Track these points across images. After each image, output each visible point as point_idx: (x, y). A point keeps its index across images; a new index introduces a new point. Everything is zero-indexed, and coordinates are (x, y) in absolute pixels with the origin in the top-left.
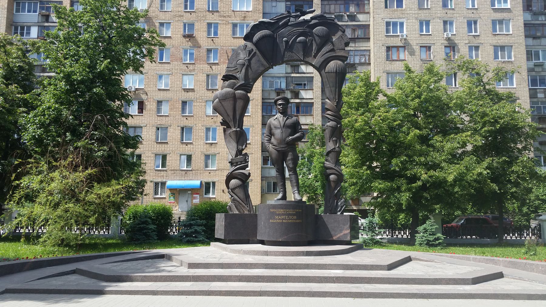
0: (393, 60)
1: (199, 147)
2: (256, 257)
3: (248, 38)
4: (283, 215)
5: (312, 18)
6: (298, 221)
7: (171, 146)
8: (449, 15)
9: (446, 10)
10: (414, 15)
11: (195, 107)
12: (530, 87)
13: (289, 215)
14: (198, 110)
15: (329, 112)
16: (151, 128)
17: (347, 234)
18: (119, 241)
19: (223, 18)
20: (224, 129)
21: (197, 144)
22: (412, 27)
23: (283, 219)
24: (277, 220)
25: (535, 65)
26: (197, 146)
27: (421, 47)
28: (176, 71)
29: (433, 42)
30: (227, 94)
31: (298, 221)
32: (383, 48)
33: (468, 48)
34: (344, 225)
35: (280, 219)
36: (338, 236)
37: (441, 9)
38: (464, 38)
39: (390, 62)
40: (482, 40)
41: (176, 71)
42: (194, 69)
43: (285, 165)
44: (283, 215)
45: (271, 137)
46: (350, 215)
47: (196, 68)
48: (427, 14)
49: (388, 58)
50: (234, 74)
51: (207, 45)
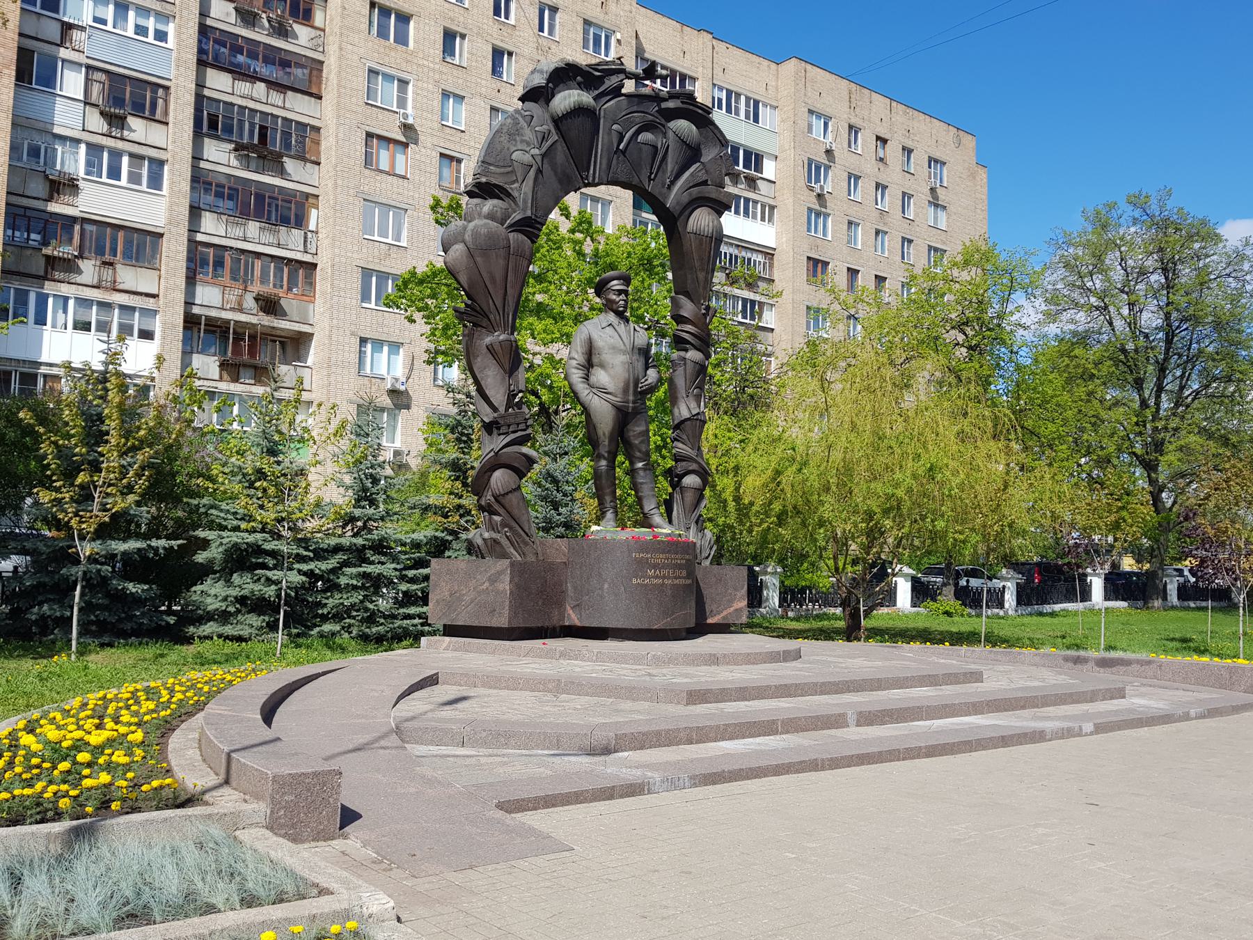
0: (381, 171)
2: (690, 670)
3: (533, 95)
4: (664, 567)
9: (499, 84)
10: (431, 74)
15: (689, 327)
18: (192, 629)
22: (425, 100)
23: (664, 577)
24: (651, 578)
27: (441, 154)
29: (467, 151)
30: (491, 236)
32: (359, 134)
34: (736, 590)
35: (657, 577)
36: (725, 613)
39: (373, 174)
44: (664, 567)
48: (460, 81)
49: (368, 161)
50: (506, 186)
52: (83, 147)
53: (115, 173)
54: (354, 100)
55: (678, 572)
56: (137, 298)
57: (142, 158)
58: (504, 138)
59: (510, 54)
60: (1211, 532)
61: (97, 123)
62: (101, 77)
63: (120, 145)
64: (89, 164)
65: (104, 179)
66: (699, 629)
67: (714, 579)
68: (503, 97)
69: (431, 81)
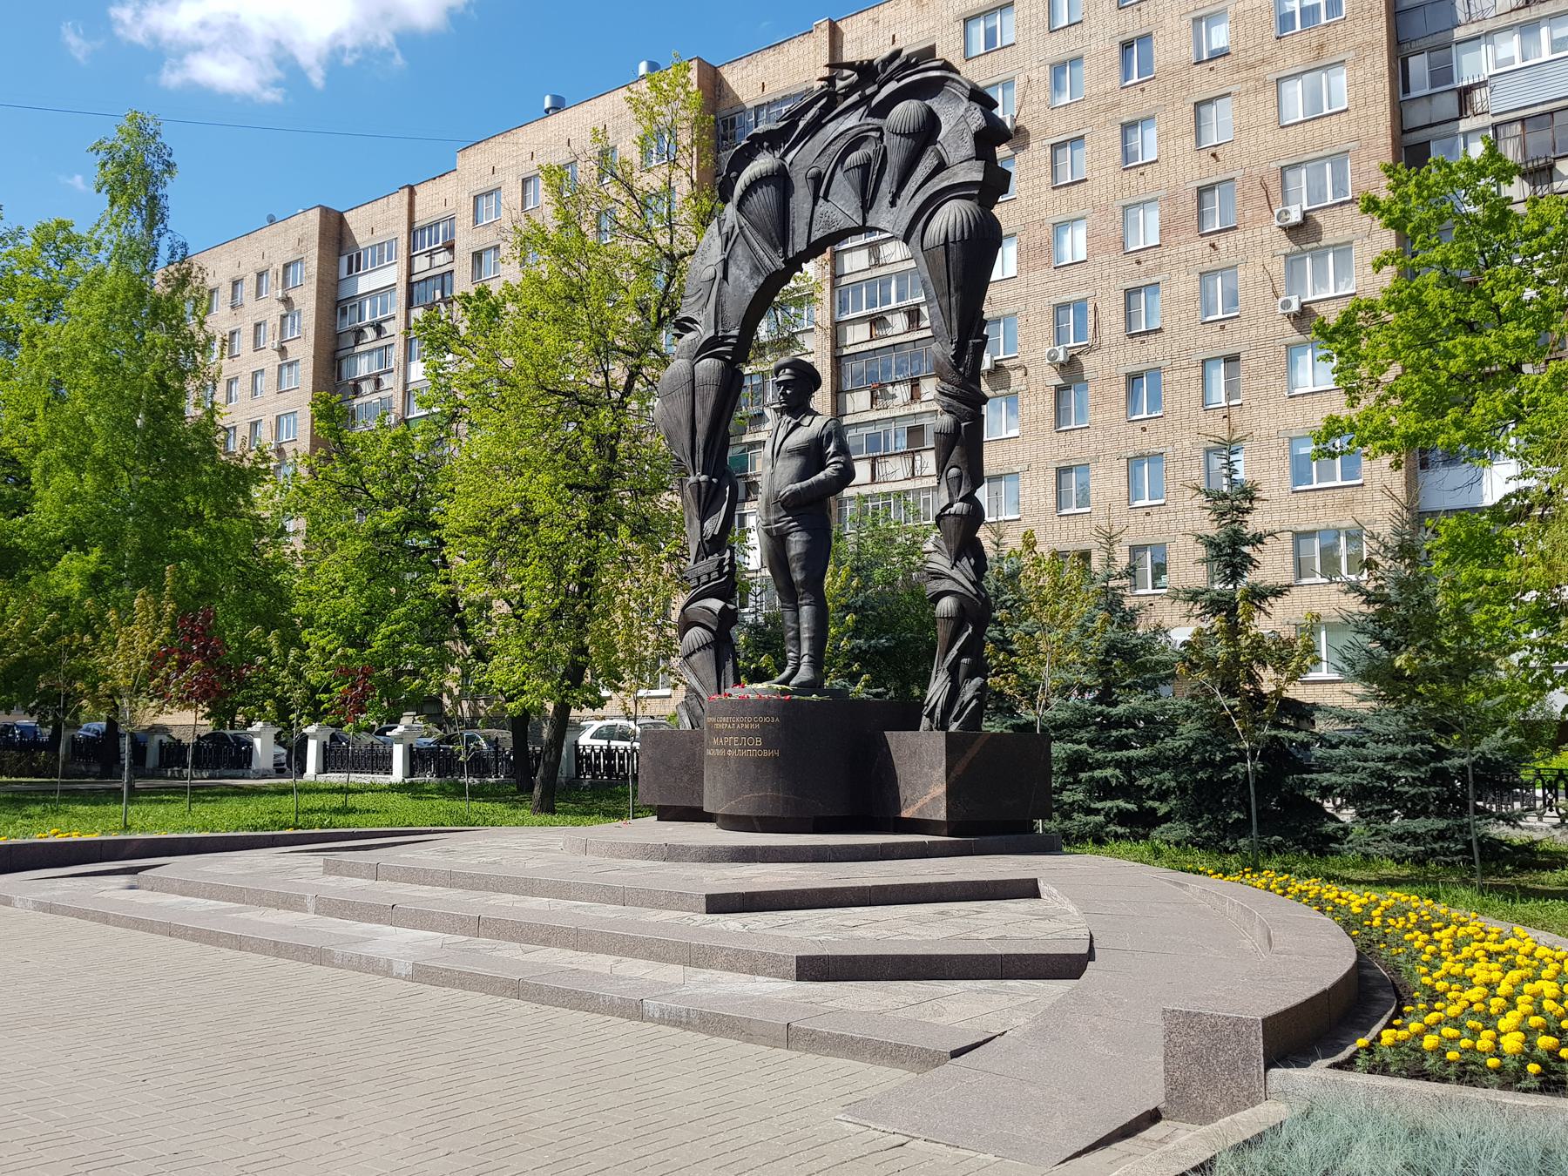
6: (765, 753)
13: (747, 733)
16: (1041, 473)
26: (1180, 516)
28: (1105, 284)
31: (765, 753)
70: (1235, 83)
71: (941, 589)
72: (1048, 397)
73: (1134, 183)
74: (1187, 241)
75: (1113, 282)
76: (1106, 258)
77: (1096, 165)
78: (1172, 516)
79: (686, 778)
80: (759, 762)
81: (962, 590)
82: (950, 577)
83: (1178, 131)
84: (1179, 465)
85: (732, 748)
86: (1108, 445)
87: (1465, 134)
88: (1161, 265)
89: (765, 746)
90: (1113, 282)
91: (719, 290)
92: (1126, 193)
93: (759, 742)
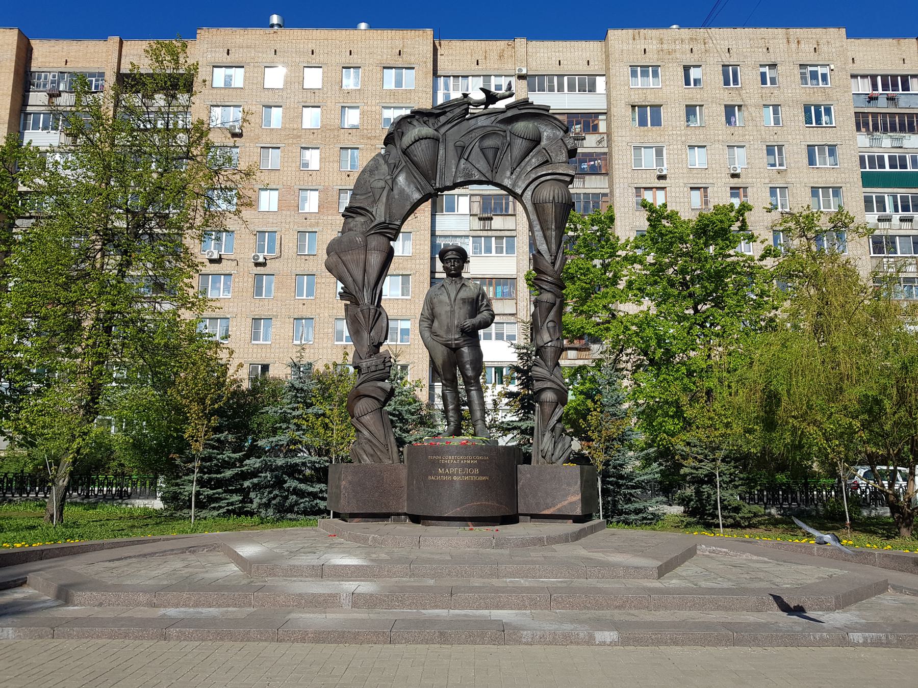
1: (325, 351)
5: (509, 107)
6: (480, 478)
7: (277, 351)
8: (737, 138)
11: (319, 285)
12: (872, 255)
13: (470, 466)
14: (323, 291)
16: (243, 319)
17: (574, 503)
19: (365, 141)
20: (346, 305)
21: (321, 346)
25: (879, 220)
26: (321, 351)
28: (287, 226)
29: (711, 181)
31: (480, 478)
33: (768, 190)
34: (569, 485)
36: (559, 506)
37: (724, 128)
38: (762, 175)
40: (791, 177)
41: (287, 226)
42: (318, 223)
43: (458, 373)
45: (433, 322)
46: (844, 511)
47: (321, 221)
51: (339, 183)
52: (493, 239)
53: (488, 250)
54: (625, 170)
55: (467, 470)
56: (505, 317)
57: (502, 237)
58: (367, 175)
59: (740, 106)
60: (82, 412)
61: (477, 224)
62: (478, 198)
63: (490, 233)
64: (475, 248)
65: (483, 254)
66: (511, 519)
67: (548, 477)
68: (737, 138)
69: (679, 143)
70: (361, 144)
71: (545, 386)
72: (250, 280)
73: (306, 179)
74: (332, 215)
75: (292, 226)
76: (288, 213)
77: (286, 164)
78: (316, 351)
79: (377, 494)
80: (477, 483)
81: (554, 386)
82: (550, 380)
83: (331, 159)
84: (322, 325)
85: (457, 475)
86: (283, 310)
87: (458, 195)
88: (318, 223)
89: (480, 474)
90: (292, 226)
91: (388, 195)
92: (302, 183)
93: (477, 471)
